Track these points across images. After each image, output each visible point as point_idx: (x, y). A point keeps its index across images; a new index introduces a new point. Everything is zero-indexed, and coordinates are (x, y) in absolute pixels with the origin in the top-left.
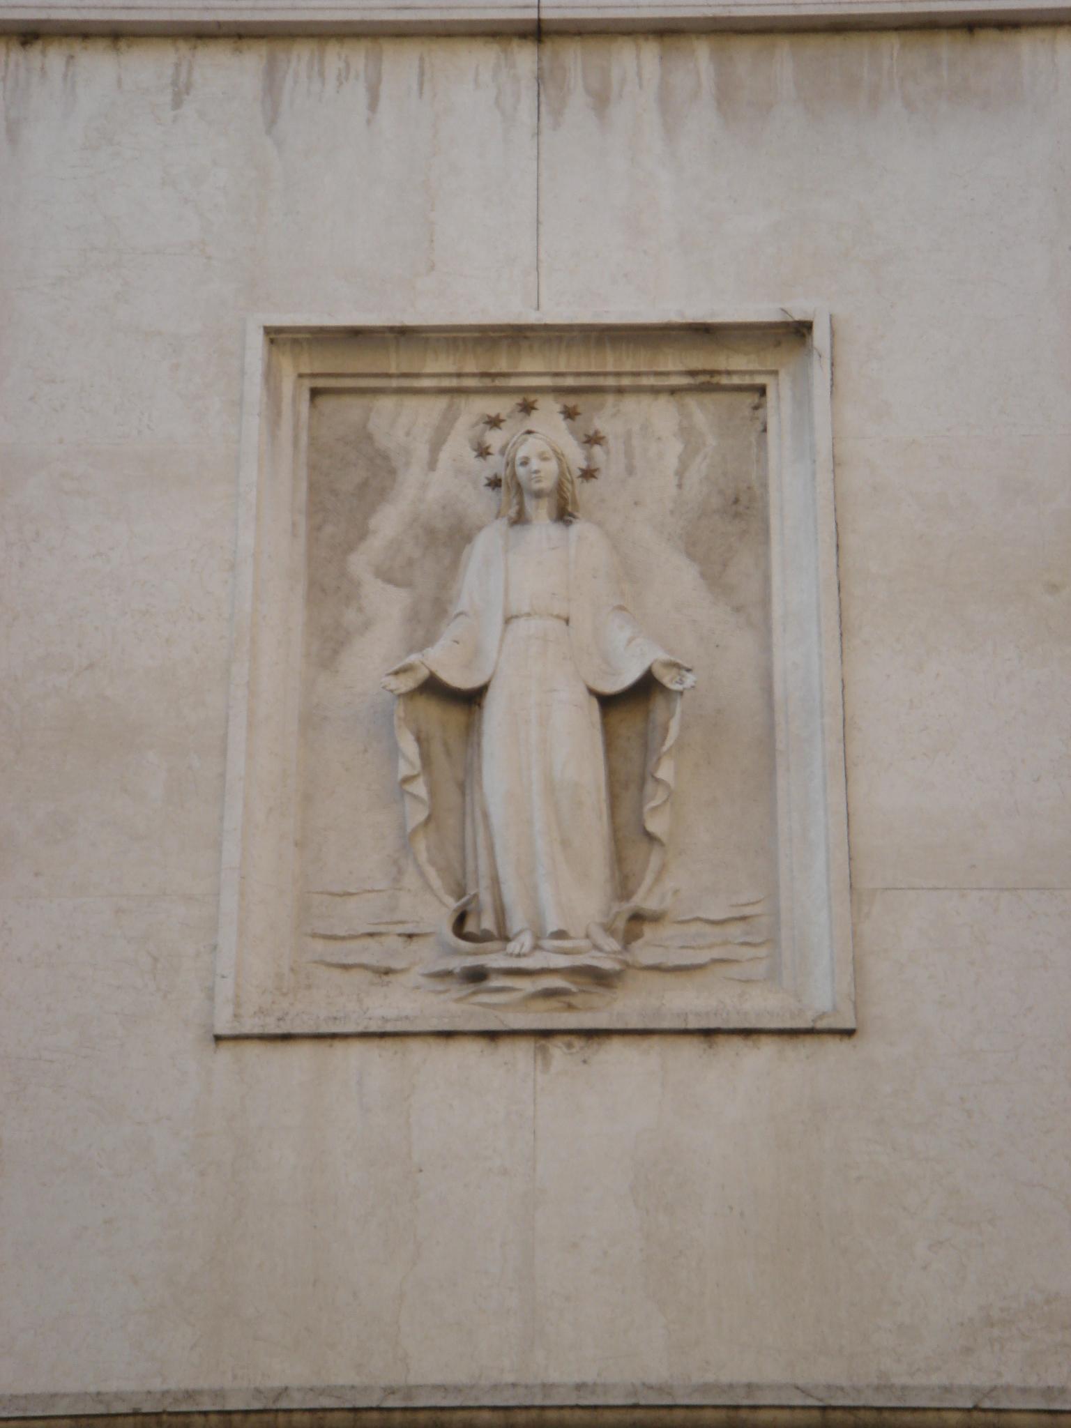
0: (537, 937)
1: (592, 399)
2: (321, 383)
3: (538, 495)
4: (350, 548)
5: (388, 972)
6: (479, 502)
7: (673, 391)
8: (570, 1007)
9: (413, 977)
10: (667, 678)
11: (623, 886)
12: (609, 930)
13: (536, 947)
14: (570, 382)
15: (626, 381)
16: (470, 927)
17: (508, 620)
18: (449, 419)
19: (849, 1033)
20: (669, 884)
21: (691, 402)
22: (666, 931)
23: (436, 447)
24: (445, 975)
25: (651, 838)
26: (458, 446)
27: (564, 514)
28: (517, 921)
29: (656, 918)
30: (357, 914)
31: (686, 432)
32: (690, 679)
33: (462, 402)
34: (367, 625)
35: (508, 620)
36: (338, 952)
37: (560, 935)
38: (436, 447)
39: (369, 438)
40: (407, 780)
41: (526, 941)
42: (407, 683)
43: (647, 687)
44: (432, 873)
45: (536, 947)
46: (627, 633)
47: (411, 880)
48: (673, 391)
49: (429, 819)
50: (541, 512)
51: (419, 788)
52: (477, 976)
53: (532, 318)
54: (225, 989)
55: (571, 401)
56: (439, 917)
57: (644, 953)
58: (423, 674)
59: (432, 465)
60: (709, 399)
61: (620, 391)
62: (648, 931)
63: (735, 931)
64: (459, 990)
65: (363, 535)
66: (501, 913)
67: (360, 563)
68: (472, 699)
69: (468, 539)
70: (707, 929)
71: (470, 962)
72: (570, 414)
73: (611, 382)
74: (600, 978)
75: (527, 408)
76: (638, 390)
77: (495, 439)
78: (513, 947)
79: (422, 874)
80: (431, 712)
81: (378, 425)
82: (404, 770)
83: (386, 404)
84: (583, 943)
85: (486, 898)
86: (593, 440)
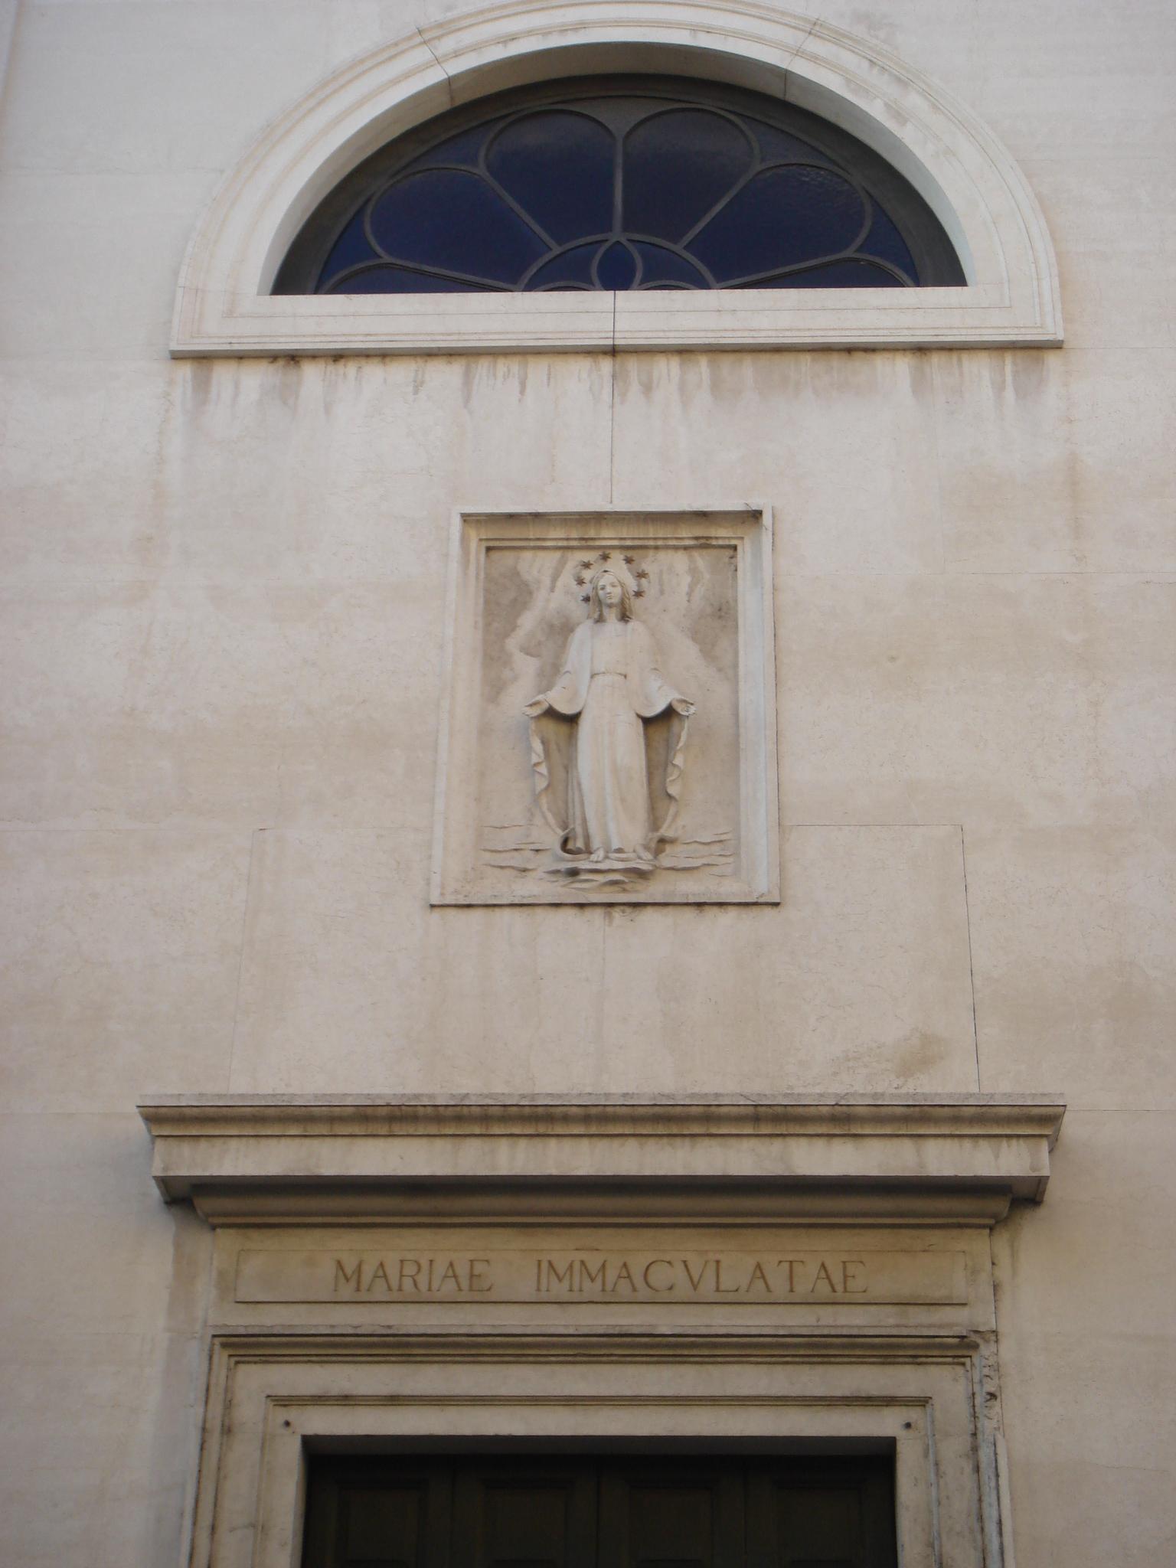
0: (607, 852)
2: (491, 544)
3: (610, 606)
5: (525, 870)
6: (578, 610)
7: (686, 548)
8: (624, 890)
11: (655, 823)
12: (646, 848)
13: (607, 857)
14: (629, 543)
15: (660, 543)
16: (570, 846)
17: (592, 676)
18: (562, 563)
19: (777, 904)
20: (680, 822)
21: (696, 554)
22: (678, 849)
24: (556, 872)
25: (670, 797)
26: (567, 579)
27: (624, 617)
28: (596, 842)
29: (672, 841)
30: (510, 838)
31: (693, 571)
32: (692, 709)
33: (569, 554)
34: (515, 678)
35: (592, 676)
36: (500, 860)
37: (619, 851)
39: (518, 574)
40: (537, 764)
41: (601, 854)
44: (549, 816)
45: (607, 857)
46: (659, 684)
47: (538, 820)
48: (686, 548)
49: (548, 786)
50: (612, 616)
52: (574, 873)
54: (436, 879)
55: (630, 554)
56: (552, 839)
57: (666, 861)
58: (545, 706)
59: (552, 589)
62: (668, 848)
64: (563, 880)
65: (514, 628)
66: (587, 838)
67: (512, 644)
68: (572, 720)
70: (701, 847)
71: (570, 865)
73: (651, 543)
74: (641, 875)
75: (605, 558)
76: (667, 547)
77: (587, 575)
78: (593, 857)
79: (545, 817)
80: (551, 727)
82: (535, 759)
83: (528, 555)
84: (632, 855)
85: (579, 830)
86: (641, 575)
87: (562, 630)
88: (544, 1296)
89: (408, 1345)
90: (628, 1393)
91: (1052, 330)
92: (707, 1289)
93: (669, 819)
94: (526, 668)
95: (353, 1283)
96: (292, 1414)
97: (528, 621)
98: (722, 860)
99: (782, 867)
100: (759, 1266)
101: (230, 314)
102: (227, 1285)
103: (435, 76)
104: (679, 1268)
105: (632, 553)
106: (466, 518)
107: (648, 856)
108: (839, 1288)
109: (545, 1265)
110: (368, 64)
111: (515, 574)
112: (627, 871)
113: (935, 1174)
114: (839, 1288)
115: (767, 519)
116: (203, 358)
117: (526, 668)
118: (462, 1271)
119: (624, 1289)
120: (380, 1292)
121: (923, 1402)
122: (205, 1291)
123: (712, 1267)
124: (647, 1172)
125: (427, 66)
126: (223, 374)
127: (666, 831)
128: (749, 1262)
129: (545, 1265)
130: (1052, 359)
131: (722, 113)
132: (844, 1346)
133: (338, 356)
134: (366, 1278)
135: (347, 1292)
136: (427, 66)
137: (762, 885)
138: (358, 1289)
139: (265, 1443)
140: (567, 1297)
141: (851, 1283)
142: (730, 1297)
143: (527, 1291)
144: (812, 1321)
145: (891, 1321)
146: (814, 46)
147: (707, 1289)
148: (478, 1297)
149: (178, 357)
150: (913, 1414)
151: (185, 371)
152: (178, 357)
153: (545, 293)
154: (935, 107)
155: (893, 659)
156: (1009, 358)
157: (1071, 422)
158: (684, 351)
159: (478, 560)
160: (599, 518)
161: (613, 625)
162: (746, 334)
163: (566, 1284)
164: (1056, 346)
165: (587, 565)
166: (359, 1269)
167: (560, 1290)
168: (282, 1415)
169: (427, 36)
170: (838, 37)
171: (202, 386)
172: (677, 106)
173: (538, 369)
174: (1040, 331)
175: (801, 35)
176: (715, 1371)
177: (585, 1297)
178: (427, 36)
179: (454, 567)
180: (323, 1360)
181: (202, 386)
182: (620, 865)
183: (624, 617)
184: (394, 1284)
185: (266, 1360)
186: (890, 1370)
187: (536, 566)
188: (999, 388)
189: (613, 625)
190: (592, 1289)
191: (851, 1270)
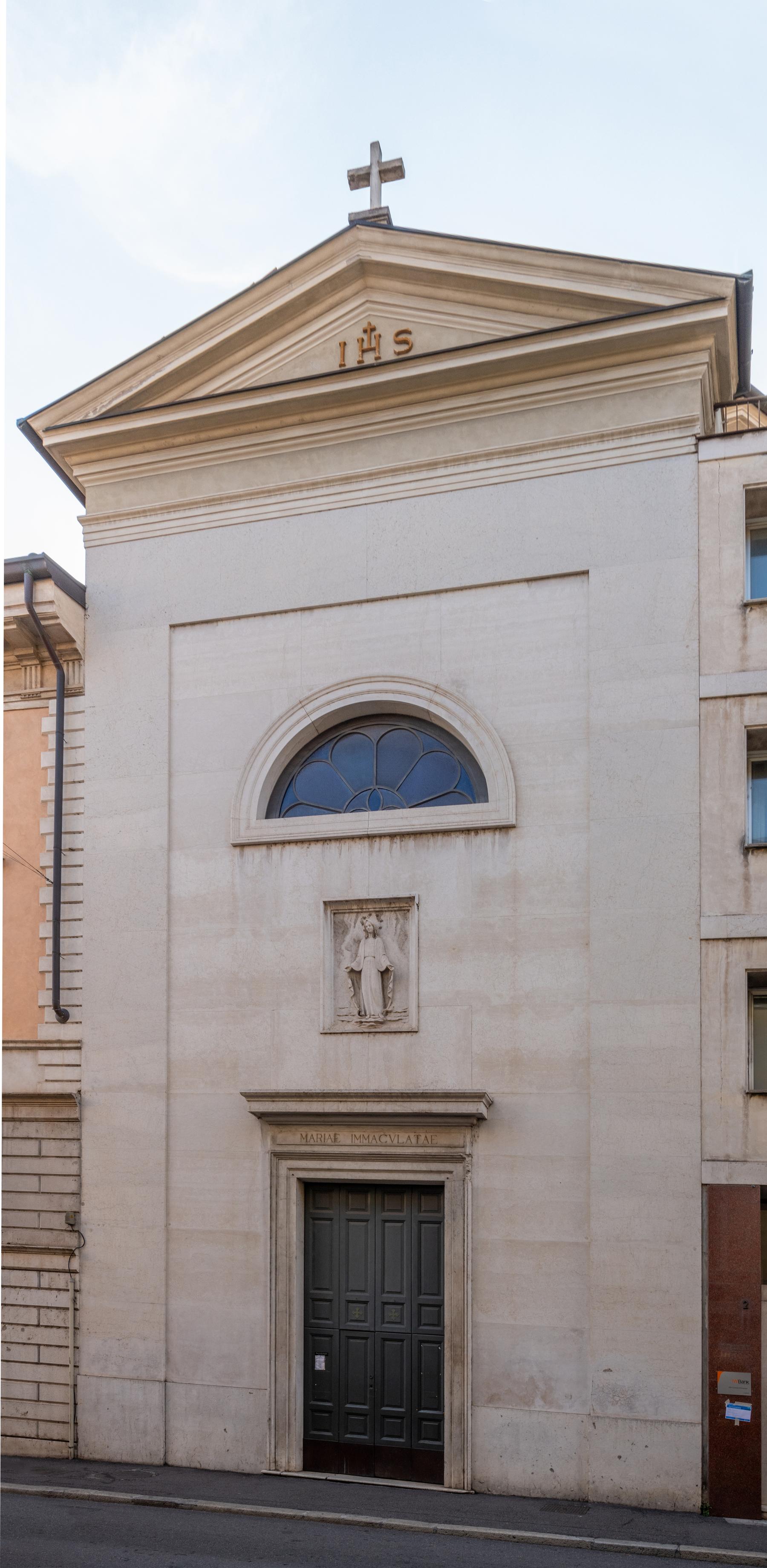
0: (370, 1015)
1: (381, 913)
2: (335, 911)
3: (370, 933)
4: (341, 944)
5: (349, 1022)
7: (395, 911)
9: (353, 1022)
10: (389, 968)
11: (385, 1006)
12: (382, 1014)
13: (370, 1017)
14: (378, 910)
17: (365, 958)
18: (357, 917)
19: (416, 1032)
20: (393, 1005)
21: (398, 913)
22: (392, 1014)
23: (355, 924)
26: (359, 923)
27: (375, 936)
28: (368, 1013)
29: (391, 1012)
30: (345, 1012)
31: (397, 919)
32: (393, 968)
35: (365, 958)
37: (374, 1015)
38: (355, 924)
41: (368, 1016)
42: (348, 970)
43: (387, 970)
45: (370, 1017)
48: (395, 911)
49: (354, 995)
50: (371, 936)
51: (352, 989)
52: (361, 1022)
53: (368, 897)
54: (321, 1025)
55: (377, 913)
56: (356, 1012)
57: (388, 1018)
58: (350, 968)
59: (354, 927)
60: (400, 912)
61: (386, 911)
62: (389, 1014)
63: (403, 1014)
65: (344, 941)
66: (365, 1013)
67: (343, 947)
68: (360, 972)
69: (360, 942)
72: (377, 916)
74: (382, 1023)
75: (370, 915)
76: (389, 911)
78: (366, 1017)
80: (354, 976)
81: (345, 919)
82: (350, 986)
83: (347, 915)
84: (377, 1017)
85: (363, 1009)
86: (382, 921)
87: (358, 942)
88: (353, 1144)
89: (426, 1158)
90: (376, 1169)
91: (512, 821)
92: (395, 1142)
93: (389, 1005)
94: (347, 954)
95: (305, 1140)
96: (296, 1173)
97: (348, 939)
98: (405, 1018)
99: (419, 1021)
100: (409, 1136)
101: (248, 827)
102: (274, 1139)
103: (307, 722)
104: (388, 1136)
105: (379, 913)
106: (325, 903)
107: (382, 1016)
108: (430, 1142)
109: (353, 1136)
110: (284, 718)
111: (343, 922)
112: (375, 1022)
113: (371, 1111)
114: (430, 1142)
115: (416, 901)
116: (242, 846)
117: (347, 954)
118: (332, 1137)
119: (374, 1142)
120: (312, 1142)
121: (451, 1172)
122: (269, 1141)
123: (397, 1136)
124: (374, 1111)
125: (304, 717)
126: (248, 851)
127: (388, 1009)
128: (407, 1135)
129: (353, 1136)
130: (512, 833)
131: (410, 730)
132: (431, 1158)
133: (284, 843)
134: (309, 1138)
135: (304, 1142)
136: (304, 717)
137: (414, 1026)
138: (307, 1141)
139: (288, 1178)
140: (359, 1144)
141: (433, 1141)
142: (402, 1145)
143: (349, 1142)
144: (423, 1151)
145: (443, 1151)
146: (438, 698)
147: (395, 1142)
148: (337, 1144)
149: (235, 846)
150: (448, 1175)
151: (238, 850)
152: (235, 846)
153: (354, 813)
154: (478, 724)
155: (454, 949)
156: (497, 833)
157: (516, 857)
158: (392, 836)
159: (331, 917)
160: (367, 901)
161: (371, 939)
162: (410, 827)
163: (359, 1140)
164: (513, 827)
165: (365, 918)
166: (306, 1136)
167: (357, 1142)
168: (292, 1172)
169: (303, 704)
170: (445, 694)
171: (242, 855)
172: (335, 740)
173: (345, 845)
174: (507, 820)
175: (432, 693)
176: (398, 1164)
177: (364, 1144)
178: (303, 704)
179: (322, 921)
180: (300, 1159)
181: (242, 855)
182: (373, 1020)
183: (375, 936)
184: (316, 1140)
185: (286, 1159)
186: (443, 1164)
187: (349, 919)
188: (493, 844)
189: (371, 939)
190: (366, 1142)
191: (433, 1137)
